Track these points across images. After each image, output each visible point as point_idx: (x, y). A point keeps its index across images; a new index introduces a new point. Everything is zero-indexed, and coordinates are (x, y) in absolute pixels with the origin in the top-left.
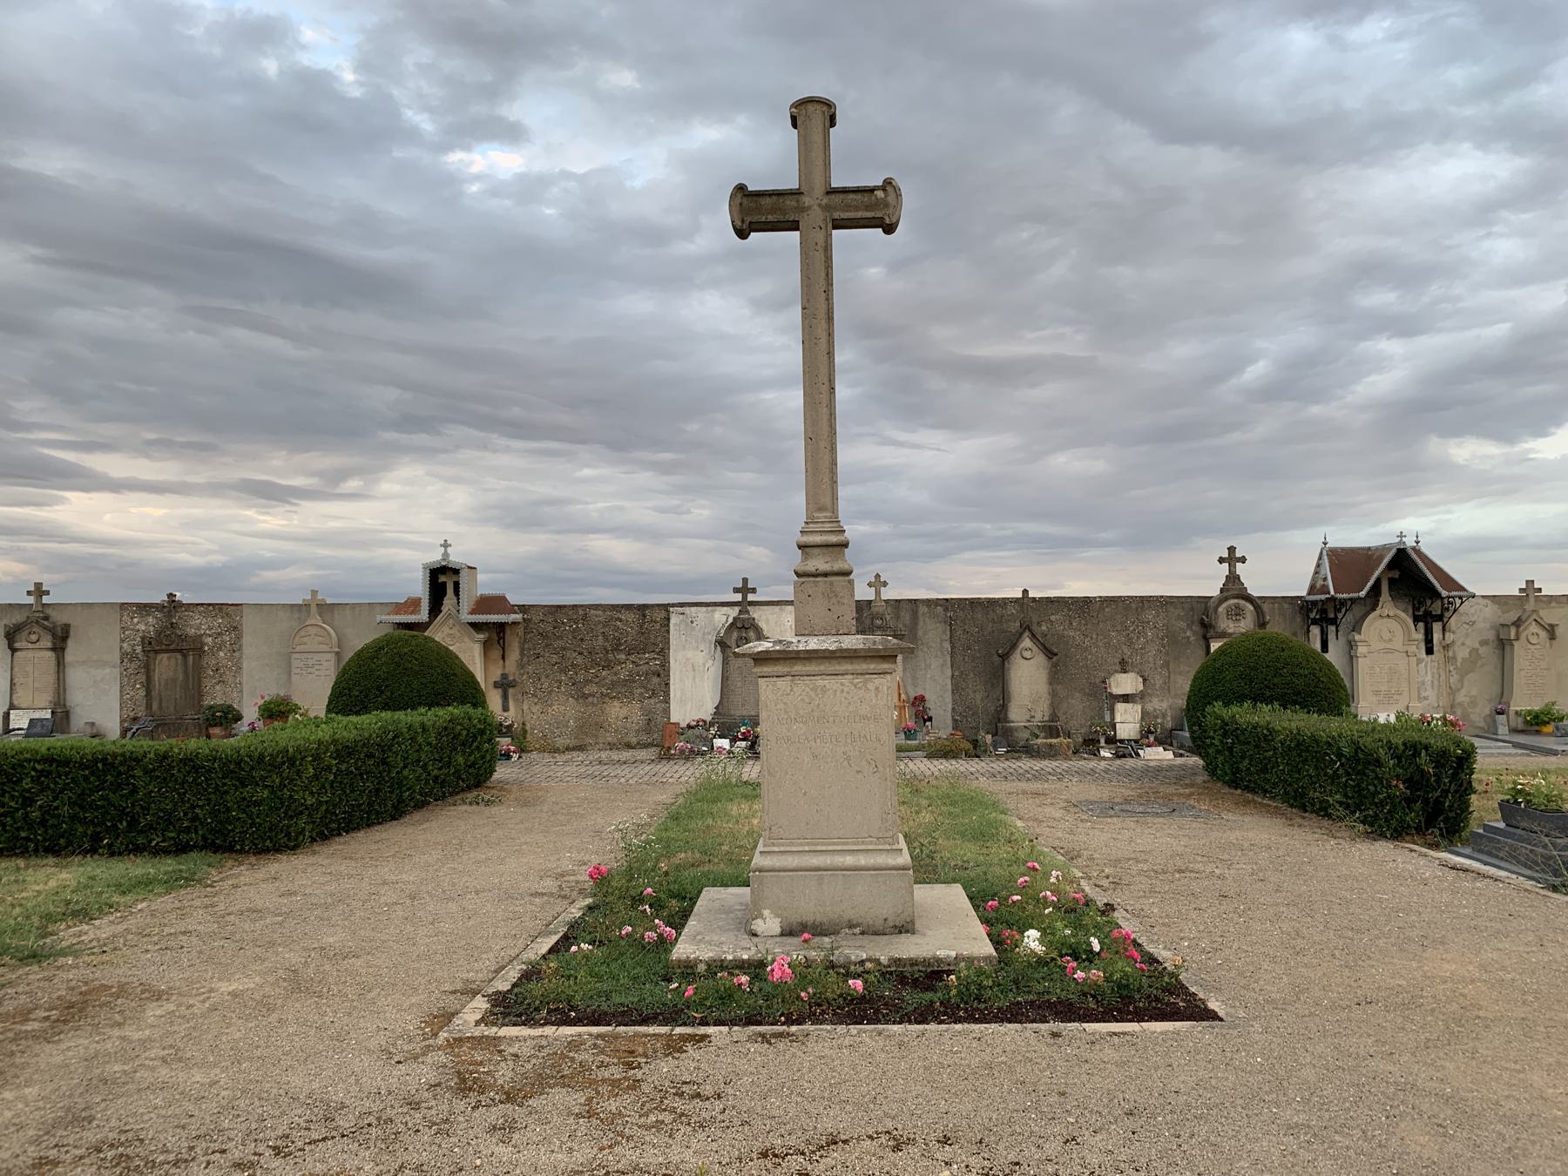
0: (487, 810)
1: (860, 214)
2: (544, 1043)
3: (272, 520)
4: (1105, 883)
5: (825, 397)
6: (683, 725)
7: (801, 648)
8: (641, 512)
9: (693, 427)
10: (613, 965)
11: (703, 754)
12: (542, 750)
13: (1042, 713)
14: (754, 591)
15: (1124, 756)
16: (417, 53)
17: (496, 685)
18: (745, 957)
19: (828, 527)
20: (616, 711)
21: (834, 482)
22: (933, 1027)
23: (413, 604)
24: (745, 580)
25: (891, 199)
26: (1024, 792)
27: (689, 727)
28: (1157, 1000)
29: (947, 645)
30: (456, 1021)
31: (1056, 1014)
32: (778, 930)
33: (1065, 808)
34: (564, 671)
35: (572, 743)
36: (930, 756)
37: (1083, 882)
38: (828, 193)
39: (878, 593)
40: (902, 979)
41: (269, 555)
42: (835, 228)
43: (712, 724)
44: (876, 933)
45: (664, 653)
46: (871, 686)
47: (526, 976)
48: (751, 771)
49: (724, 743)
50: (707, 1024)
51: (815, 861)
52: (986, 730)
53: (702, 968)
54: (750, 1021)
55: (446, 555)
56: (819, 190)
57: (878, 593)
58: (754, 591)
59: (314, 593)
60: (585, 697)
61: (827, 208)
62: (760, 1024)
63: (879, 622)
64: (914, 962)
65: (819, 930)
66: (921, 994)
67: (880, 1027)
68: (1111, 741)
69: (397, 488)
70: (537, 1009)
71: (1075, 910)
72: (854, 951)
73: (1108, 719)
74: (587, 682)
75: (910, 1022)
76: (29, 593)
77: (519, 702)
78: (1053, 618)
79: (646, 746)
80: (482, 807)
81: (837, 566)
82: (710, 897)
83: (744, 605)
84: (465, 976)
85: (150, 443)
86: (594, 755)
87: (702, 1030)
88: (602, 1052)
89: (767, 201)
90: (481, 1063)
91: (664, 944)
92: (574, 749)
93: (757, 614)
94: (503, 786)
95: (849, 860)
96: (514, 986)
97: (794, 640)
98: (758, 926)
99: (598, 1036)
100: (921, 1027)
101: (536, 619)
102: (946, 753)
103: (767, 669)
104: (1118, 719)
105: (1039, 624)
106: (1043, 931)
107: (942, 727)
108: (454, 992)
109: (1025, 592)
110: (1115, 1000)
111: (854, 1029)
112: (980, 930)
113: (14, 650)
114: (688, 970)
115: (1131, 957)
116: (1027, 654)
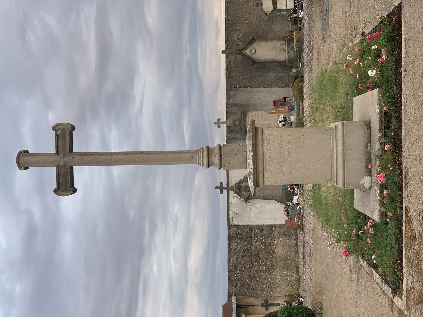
0: (325, 309)
1: (67, 141)
2: (408, 272)
4: (354, 33)
5: (145, 156)
6: (286, 218)
7: (252, 167)
8: (176, 241)
9: (132, 214)
10: (383, 246)
11: (300, 209)
12: (298, 287)
13: (282, 45)
14: (222, 184)
15: (302, 6)
17: (267, 309)
18: (378, 191)
19: (200, 155)
20: (280, 251)
21: (181, 152)
22: (403, 117)
24: (217, 188)
25: (61, 127)
26: (318, 58)
27: (288, 215)
28: (394, 26)
29: (249, 89)
30: (401, 308)
31: (399, 68)
32: (369, 177)
33: (325, 41)
35: (295, 272)
36: (302, 100)
37: (354, 43)
38: (58, 154)
39: (223, 123)
40: (387, 127)
42: (72, 151)
43: (286, 204)
45: (252, 228)
46: (268, 138)
47: (387, 283)
48: (308, 187)
49: (295, 198)
50: (402, 207)
52: (290, 71)
53: (383, 209)
54: (401, 190)
56: (57, 158)
57: (223, 123)
58: (222, 184)
60: (273, 266)
61: (65, 155)
62: (402, 186)
63: (237, 123)
64: (381, 122)
65: (369, 160)
66: (391, 119)
67: (403, 138)
68: (295, 11)
70: (397, 276)
71: (363, 54)
72: (376, 146)
73: (284, 13)
74: (265, 265)
75: (401, 126)
77: (275, 298)
78: (235, 39)
79: (297, 237)
80: (323, 312)
81: (217, 151)
82: (357, 206)
83: (229, 188)
84: (387, 307)
86: (301, 261)
87: (404, 209)
88: (411, 248)
89: (61, 180)
90: (414, 296)
91: (374, 225)
93: (233, 182)
94: (315, 303)
95: (340, 147)
96: (390, 287)
97: (249, 170)
98: (367, 185)
99: (406, 251)
100: (403, 122)
101: (235, 290)
102: (300, 93)
103: (261, 181)
104: (284, 8)
105: (238, 45)
106: (370, 68)
107: (288, 92)
108: (392, 311)
109: (223, 52)
110: (394, 43)
111: (404, 149)
112: (370, 93)
114: (383, 215)
115: (377, 36)
116: (253, 51)
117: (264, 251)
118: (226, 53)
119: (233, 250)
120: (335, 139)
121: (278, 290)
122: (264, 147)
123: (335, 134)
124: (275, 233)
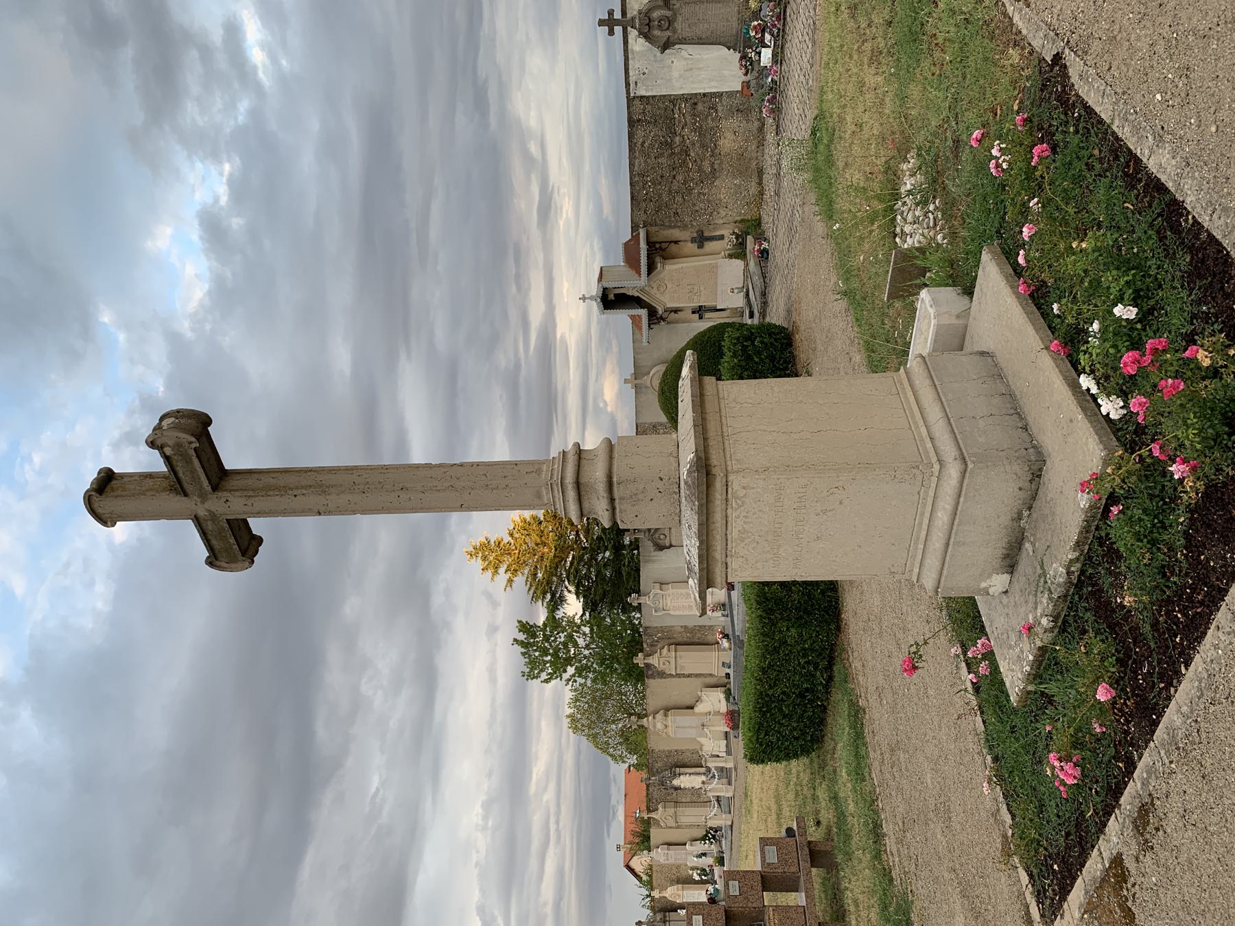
3: (566, 208)
12: (759, 206)
14: (611, 13)
16: (191, 113)
19: (558, 495)
20: (727, 143)
23: (636, 320)
24: (602, 23)
32: (1006, 577)
34: (690, 190)
35: (755, 179)
41: (591, 206)
44: (1034, 498)
45: (673, 100)
46: (741, 493)
51: (937, 543)
55: (591, 298)
58: (611, 13)
59: (626, 381)
69: (533, 113)
74: (700, 170)
76: (611, 33)
83: (626, 24)
85: (519, 289)
92: (760, 178)
95: (942, 517)
101: (644, 217)
113: (671, 546)
117: (698, 145)
118: (609, 19)
119: (639, 145)
120: (931, 493)
121: (723, 213)
122: (729, 511)
123: (933, 485)
124: (720, 109)
